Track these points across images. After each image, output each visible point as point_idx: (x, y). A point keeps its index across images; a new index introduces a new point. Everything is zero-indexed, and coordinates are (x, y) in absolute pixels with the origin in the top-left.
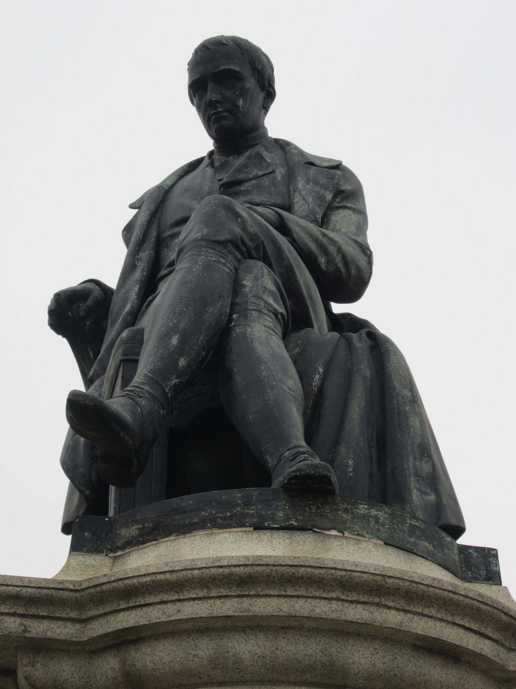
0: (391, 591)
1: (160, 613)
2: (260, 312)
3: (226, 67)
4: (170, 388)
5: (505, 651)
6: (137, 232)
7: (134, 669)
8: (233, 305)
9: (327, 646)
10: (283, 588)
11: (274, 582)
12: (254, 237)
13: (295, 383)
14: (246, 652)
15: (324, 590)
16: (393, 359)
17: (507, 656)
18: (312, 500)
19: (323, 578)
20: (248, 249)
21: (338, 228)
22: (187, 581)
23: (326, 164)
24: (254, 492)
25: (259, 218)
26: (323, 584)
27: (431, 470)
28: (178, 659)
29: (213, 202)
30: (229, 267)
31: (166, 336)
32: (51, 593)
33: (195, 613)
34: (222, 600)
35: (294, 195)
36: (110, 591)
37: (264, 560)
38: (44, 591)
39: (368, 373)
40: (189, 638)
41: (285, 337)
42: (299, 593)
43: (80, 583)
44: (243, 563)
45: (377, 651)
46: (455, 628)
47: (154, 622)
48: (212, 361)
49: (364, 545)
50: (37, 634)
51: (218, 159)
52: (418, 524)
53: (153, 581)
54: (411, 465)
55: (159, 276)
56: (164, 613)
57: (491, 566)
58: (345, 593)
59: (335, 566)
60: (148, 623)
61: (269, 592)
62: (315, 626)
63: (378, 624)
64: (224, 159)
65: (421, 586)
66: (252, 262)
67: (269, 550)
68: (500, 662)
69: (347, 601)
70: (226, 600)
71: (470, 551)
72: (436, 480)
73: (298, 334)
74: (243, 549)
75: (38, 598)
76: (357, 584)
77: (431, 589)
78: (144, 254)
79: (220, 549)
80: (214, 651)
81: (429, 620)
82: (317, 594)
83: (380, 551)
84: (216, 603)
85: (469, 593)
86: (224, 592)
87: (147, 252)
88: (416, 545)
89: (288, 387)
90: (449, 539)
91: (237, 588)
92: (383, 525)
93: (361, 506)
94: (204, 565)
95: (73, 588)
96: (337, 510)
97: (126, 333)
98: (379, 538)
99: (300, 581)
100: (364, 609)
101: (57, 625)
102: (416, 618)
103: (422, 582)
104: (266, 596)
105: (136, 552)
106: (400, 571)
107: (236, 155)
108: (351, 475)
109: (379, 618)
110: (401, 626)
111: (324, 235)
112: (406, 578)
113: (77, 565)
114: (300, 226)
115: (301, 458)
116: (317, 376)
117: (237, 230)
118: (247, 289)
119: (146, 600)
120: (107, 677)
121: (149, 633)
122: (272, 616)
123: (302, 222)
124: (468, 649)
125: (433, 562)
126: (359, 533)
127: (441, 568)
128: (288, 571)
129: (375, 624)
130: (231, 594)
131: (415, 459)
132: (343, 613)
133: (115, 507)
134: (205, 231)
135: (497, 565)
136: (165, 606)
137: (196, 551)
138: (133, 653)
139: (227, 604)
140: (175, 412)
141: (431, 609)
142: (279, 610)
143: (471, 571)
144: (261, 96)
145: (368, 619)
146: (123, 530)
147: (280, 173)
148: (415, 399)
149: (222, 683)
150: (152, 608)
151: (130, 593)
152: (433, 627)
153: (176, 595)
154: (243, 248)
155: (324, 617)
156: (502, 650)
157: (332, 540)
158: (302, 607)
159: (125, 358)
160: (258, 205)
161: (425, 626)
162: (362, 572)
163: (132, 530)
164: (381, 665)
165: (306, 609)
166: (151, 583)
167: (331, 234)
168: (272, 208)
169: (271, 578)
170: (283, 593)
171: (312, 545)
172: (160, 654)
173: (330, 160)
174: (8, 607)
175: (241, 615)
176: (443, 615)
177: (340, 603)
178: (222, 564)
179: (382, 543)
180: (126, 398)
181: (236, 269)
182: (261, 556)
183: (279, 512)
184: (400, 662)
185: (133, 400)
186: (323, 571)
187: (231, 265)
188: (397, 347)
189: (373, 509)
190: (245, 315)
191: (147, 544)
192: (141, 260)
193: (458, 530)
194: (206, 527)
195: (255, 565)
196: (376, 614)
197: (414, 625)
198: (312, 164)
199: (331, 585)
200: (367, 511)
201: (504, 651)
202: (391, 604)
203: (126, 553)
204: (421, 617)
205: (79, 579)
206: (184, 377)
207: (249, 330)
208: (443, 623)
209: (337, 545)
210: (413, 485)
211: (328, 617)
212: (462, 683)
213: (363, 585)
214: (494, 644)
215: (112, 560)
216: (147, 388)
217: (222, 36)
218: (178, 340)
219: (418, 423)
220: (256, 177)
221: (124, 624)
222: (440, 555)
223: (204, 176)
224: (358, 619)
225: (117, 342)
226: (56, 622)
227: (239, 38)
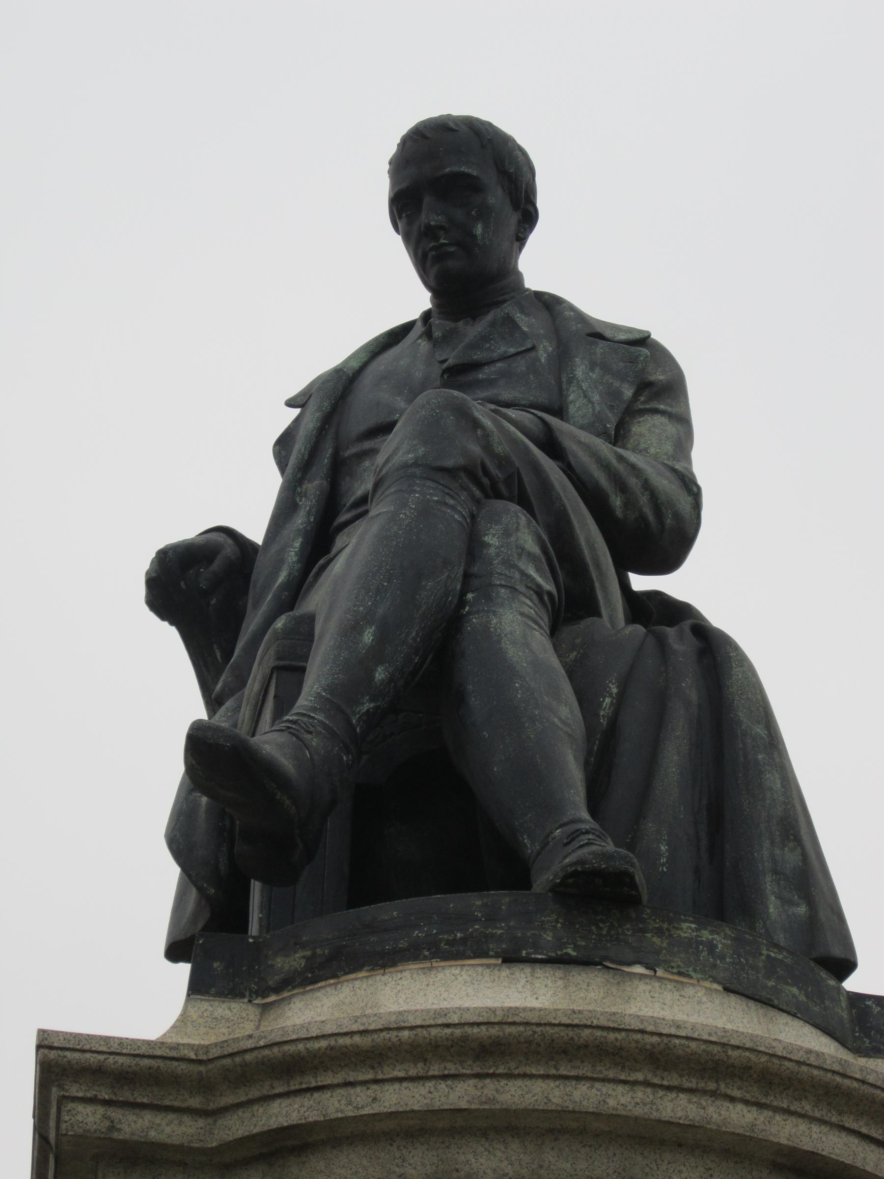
1: (343, 1102)
2: (513, 589)
3: (456, 169)
4: (360, 717)
6: (299, 448)
8: (467, 576)
10: (553, 1063)
11: (538, 1053)
12: (503, 462)
13: (572, 712)
14: (489, 1171)
15: (623, 1067)
16: (737, 672)
18: (600, 915)
19: (621, 1048)
20: (493, 482)
21: (643, 446)
22: (390, 1048)
23: (622, 337)
24: (504, 899)
25: (512, 429)
26: (621, 1057)
27: (800, 864)
29: (435, 401)
30: (460, 513)
31: (353, 629)
32: (157, 1065)
33: (402, 1103)
34: (449, 1082)
35: (568, 389)
37: (521, 1015)
38: (146, 1062)
39: (694, 696)
40: (391, 1145)
41: (554, 631)
42: (580, 1072)
43: (207, 1048)
44: (486, 1020)
45: (711, 1172)
46: (843, 1134)
47: (332, 1117)
48: (431, 672)
49: (690, 991)
51: (439, 326)
52: (780, 957)
53: (332, 1048)
54: (766, 853)
55: (336, 523)
56: (350, 1103)
58: (658, 1072)
59: (641, 1027)
60: (322, 1119)
63: (714, 1127)
64: (449, 325)
66: (499, 504)
67: (529, 998)
69: (661, 1087)
70: (456, 1082)
71: (869, 1003)
72: (809, 880)
73: (575, 627)
74: (484, 995)
77: (804, 1068)
78: (310, 485)
79: (445, 995)
80: (434, 1168)
81: (800, 1121)
82: (611, 1074)
85: (868, 1076)
86: (452, 1068)
87: (317, 482)
89: (560, 719)
90: (832, 982)
91: (474, 1062)
92: (722, 957)
93: (685, 925)
94: (419, 1023)
95: (193, 1056)
96: (644, 931)
97: (283, 622)
98: (715, 980)
100: (690, 1101)
102: (778, 1118)
103: (789, 1056)
104: (525, 1076)
106: (752, 1037)
107: (469, 319)
108: (665, 869)
109: (715, 1116)
110: (753, 1131)
111: (621, 458)
112: (762, 1049)
113: (201, 1017)
114: (579, 442)
115: (583, 840)
116: (608, 700)
117: (476, 449)
118: (492, 551)
119: (319, 1079)
122: (535, 1110)
123: (585, 436)
124: (864, 1170)
125: (805, 1021)
126: (682, 970)
127: (819, 1033)
128: (562, 1034)
129: (708, 1126)
130: (465, 1071)
131: (772, 843)
132: (654, 1107)
133: (260, 919)
134: (421, 451)
137: (404, 997)
139: (457, 1089)
140: (365, 757)
141: (804, 1102)
142: (545, 1100)
143: (868, 1036)
144: (513, 219)
145: (697, 1118)
146: (279, 960)
147: (546, 351)
148: (773, 742)
150: (329, 1094)
151: (294, 1066)
152: (807, 1133)
153: (371, 1071)
154: (486, 481)
155: (623, 1113)
157: (636, 982)
158: (585, 1096)
159: (282, 663)
160: (508, 405)
161: (794, 1130)
162: (687, 1038)
163: (295, 960)
165: (591, 1100)
166: (328, 1051)
167: (633, 458)
168: (533, 411)
170: (553, 1072)
171: (602, 991)
172: (343, 1172)
173: (630, 330)
174: (84, 1088)
175: (482, 1107)
176: (824, 1113)
178: (450, 1021)
179: (720, 988)
180: (286, 733)
181: (473, 517)
182: (517, 1008)
183: (545, 933)
185: (297, 737)
186: (620, 1036)
187: (464, 509)
188: (743, 652)
189: (706, 929)
190: (487, 594)
191: (320, 985)
192: (305, 496)
193: (845, 966)
194: (422, 956)
195: (506, 1023)
196: (711, 1109)
198: (599, 336)
200: (695, 934)
202: (737, 1093)
203: (283, 999)
206: (384, 700)
207: (495, 621)
208: (823, 1127)
209: (644, 992)
210: (769, 888)
211: (629, 1114)
215: (260, 1010)
216: (320, 717)
217: (449, 116)
218: (374, 635)
219: (778, 782)
220: (504, 358)
221: (280, 1120)
222: (817, 1009)
223: (415, 355)
224: (680, 1118)
225: (266, 637)
226: (164, 1114)
227: (477, 120)
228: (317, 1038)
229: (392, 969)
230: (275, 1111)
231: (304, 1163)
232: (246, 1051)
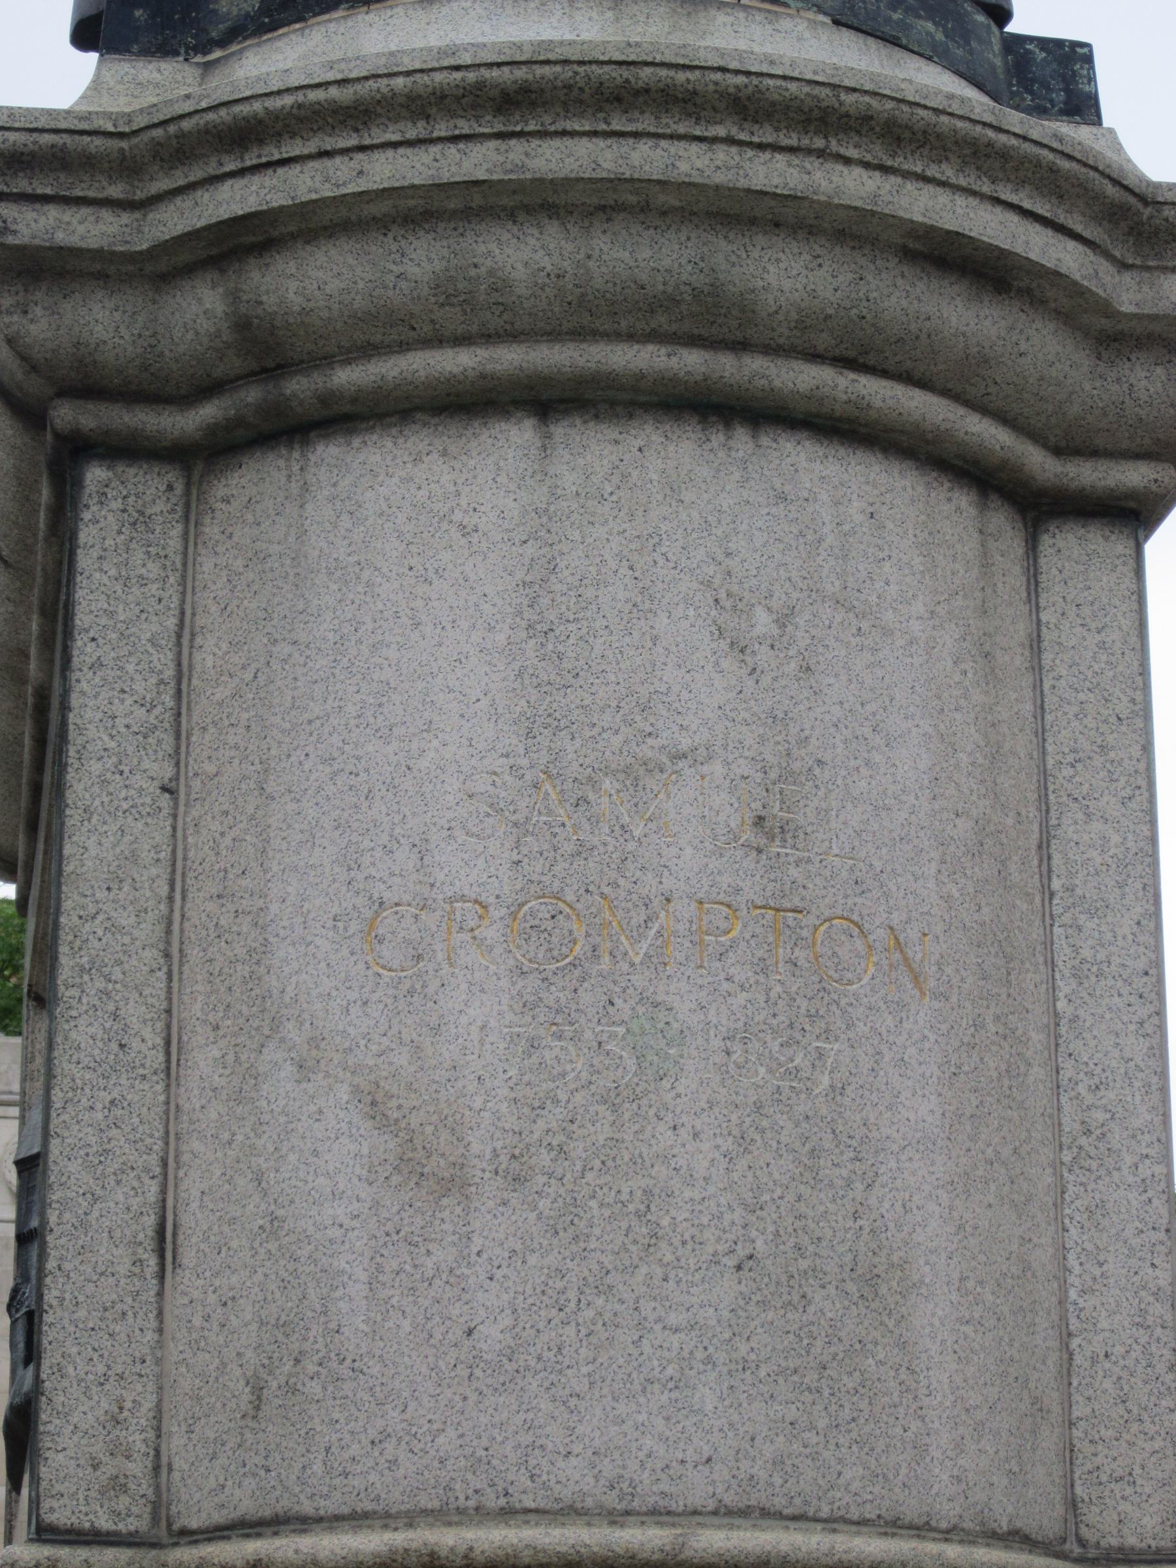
0: (852, 123)
1: (318, 178)
5: (1112, 269)
7: (259, 311)
9: (705, 249)
10: (601, 115)
11: (581, 102)
14: (519, 266)
15: (698, 119)
17: (1117, 279)
28: (361, 285)
34: (461, 146)
36: (199, 132)
38: (47, 139)
43: (129, 118)
45: (820, 260)
46: (998, 209)
49: (786, 24)
50: (34, 237)
53: (300, 106)
56: (327, 180)
57: (1077, 83)
58: (746, 125)
59: (722, 63)
61: (569, 125)
62: (677, 203)
63: (823, 198)
65: (922, 112)
68: (1100, 292)
69: (750, 144)
75: (32, 154)
76: (773, 104)
77: (944, 119)
80: (444, 263)
81: (940, 190)
82: (681, 129)
83: (824, 38)
84: (447, 152)
86: (464, 127)
88: (905, 27)
94: (418, 66)
95: (112, 129)
98: (820, 10)
99: (641, 99)
101: (78, 216)
102: (910, 186)
104: (564, 133)
105: (256, 49)
106: (873, 77)
109: (824, 184)
112: (887, 92)
113: (121, 82)
119: (283, 149)
120: (197, 334)
121: (292, 228)
128: (614, 75)
132: (741, 172)
135: (1092, 79)
136: (327, 163)
138: (256, 275)
139: (474, 154)
141: (944, 166)
143: (1031, 92)
145: (800, 187)
149: (464, 339)
151: (245, 136)
153: (355, 135)
155: (699, 180)
156: (1105, 266)
158: (646, 159)
161: (931, 203)
162: (784, 78)
164: (828, 294)
166: (295, 111)
169: (576, 92)
170: (603, 127)
172: (320, 274)
176: (972, 180)
177: (734, 150)
178: (460, 62)
179: (827, 20)
184: (873, 286)
186: (693, 76)
191: (281, 32)
195: (536, 62)
196: (819, 174)
197: (904, 202)
199: (714, 108)
201: (1111, 268)
202: (852, 153)
203: (232, 54)
204: (921, 185)
205: (127, 110)
208: (970, 199)
211: (706, 181)
212: (1014, 338)
213: (788, 107)
214: (1088, 251)
221: (234, 207)
222: (960, 52)
228: (279, 92)
229: (378, 5)
230: (225, 196)
231: (267, 265)
232: (182, 117)
